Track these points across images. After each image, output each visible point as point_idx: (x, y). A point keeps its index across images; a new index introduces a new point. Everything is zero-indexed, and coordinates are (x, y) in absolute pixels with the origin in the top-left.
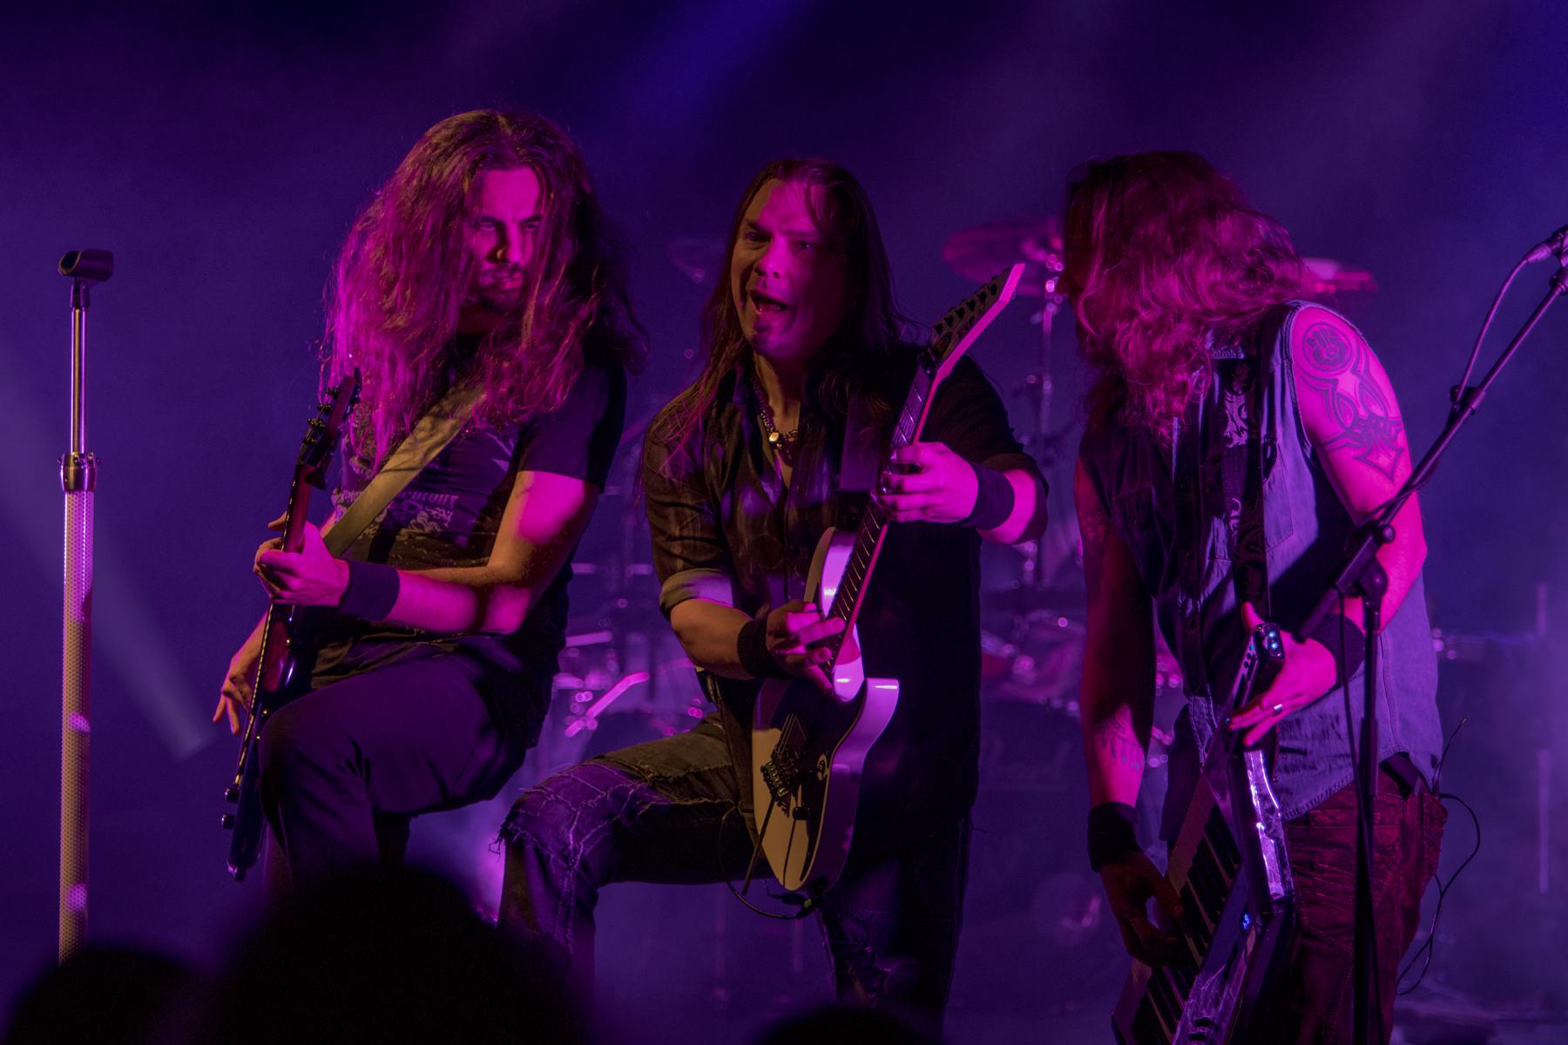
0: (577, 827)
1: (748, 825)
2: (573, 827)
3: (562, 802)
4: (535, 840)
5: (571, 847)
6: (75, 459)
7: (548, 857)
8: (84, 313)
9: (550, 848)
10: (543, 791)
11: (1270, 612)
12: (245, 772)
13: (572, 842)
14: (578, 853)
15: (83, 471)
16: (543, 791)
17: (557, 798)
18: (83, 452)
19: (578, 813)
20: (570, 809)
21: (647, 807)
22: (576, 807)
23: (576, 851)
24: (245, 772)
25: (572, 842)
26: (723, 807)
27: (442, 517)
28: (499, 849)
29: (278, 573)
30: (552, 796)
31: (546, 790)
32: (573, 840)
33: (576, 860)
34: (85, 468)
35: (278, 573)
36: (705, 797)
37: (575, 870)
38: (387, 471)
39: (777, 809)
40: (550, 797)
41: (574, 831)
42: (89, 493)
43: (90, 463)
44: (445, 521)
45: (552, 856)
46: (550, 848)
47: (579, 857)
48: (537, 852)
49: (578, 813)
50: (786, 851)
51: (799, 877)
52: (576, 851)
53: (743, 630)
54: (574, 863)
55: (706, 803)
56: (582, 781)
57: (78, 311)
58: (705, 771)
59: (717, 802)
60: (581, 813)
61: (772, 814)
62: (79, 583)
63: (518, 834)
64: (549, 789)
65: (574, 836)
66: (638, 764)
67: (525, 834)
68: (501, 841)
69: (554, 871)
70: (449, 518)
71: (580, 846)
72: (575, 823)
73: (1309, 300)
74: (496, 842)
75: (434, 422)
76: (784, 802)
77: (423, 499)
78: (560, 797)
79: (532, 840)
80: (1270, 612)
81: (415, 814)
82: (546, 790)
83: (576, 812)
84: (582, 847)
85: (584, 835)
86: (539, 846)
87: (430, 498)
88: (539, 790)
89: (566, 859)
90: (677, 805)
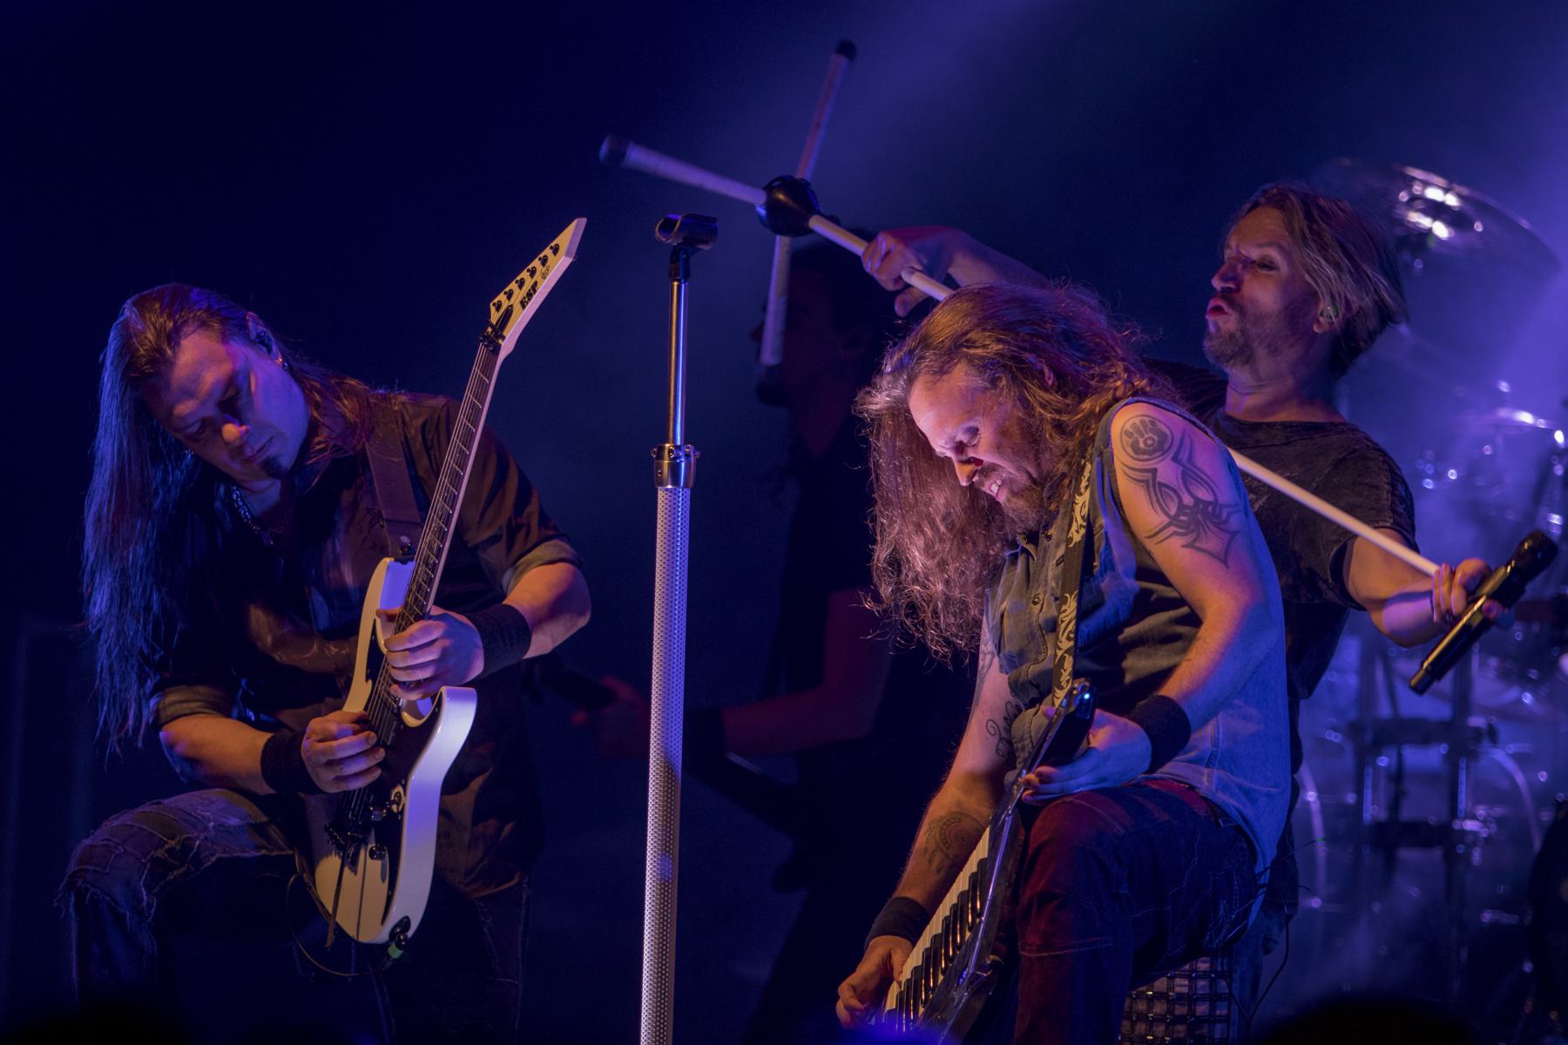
5: (144, 904)
6: (670, 451)
8: (683, 286)
10: (110, 843)
15: (679, 464)
16: (110, 843)
17: (125, 851)
18: (679, 443)
19: (148, 866)
21: (213, 859)
30: (120, 847)
33: (150, 914)
34: (681, 462)
38: (196, 422)
40: (117, 848)
42: (685, 490)
43: (687, 456)
49: (148, 866)
50: (364, 900)
51: (380, 922)
57: (676, 283)
62: (672, 573)
64: (116, 840)
66: (198, 811)
73: (758, 352)
90: (238, 857)
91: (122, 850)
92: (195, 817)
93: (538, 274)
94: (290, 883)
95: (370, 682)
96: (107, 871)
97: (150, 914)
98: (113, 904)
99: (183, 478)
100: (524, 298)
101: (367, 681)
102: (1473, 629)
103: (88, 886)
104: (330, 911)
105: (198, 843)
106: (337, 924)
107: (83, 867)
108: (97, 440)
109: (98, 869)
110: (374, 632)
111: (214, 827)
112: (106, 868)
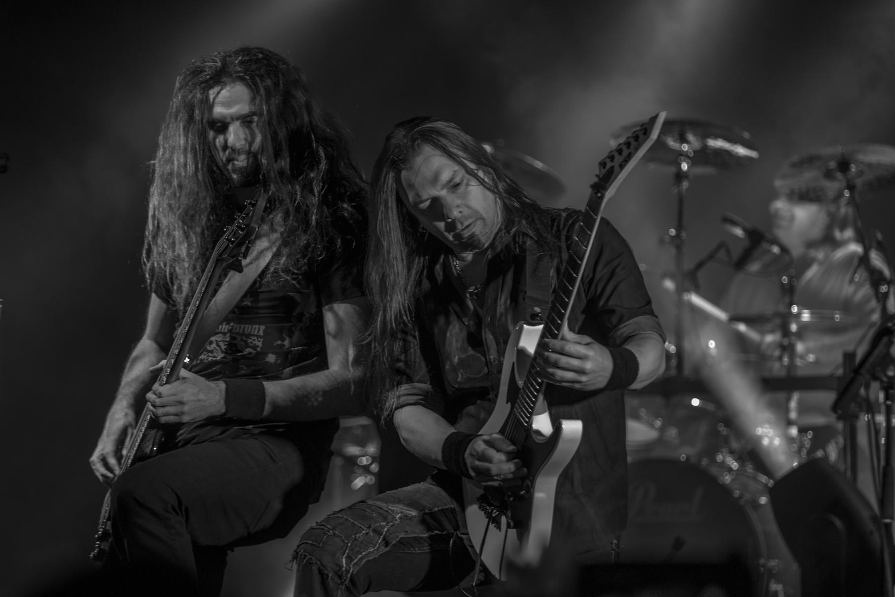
0: (348, 554)
1: (466, 542)
2: (346, 555)
3: (338, 536)
4: (319, 563)
5: (344, 569)
7: (328, 576)
9: (330, 570)
10: (325, 528)
11: (525, 199)
12: (111, 520)
13: (345, 565)
14: (348, 573)
16: (325, 528)
17: (334, 534)
19: (349, 544)
20: (344, 541)
22: (347, 540)
23: (347, 571)
24: (111, 520)
25: (345, 565)
26: (449, 536)
27: (255, 344)
28: (292, 567)
29: (510, 276)
30: (331, 531)
31: (326, 527)
32: (346, 563)
33: (347, 577)
35: (510, 276)
36: (436, 530)
37: (346, 585)
39: (492, 526)
40: (329, 532)
41: (346, 557)
44: (258, 346)
45: (330, 575)
46: (330, 570)
47: (349, 576)
48: (320, 572)
52: (347, 571)
53: (447, 439)
54: (345, 580)
55: (437, 534)
56: (352, 521)
58: (436, 512)
59: (444, 533)
60: (351, 544)
61: (480, 542)
63: (306, 559)
64: (329, 526)
65: (346, 561)
67: (311, 558)
68: (293, 561)
69: (331, 585)
70: (260, 344)
71: (350, 568)
72: (347, 551)
74: (290, 562)
75: (768, 241)
76: (496, 522)
77: (241, 332)
78: (336, 532)
79: (316, 564)
80: (525, 199)
81: (232, 545)
82: (326, 527)
83: (348, 544)
84: (352, 569)
85: (352, 560)
86: (321, 567)
87: (246, 330)
88: (322, 527)
89: (340, 577)
91: (332, 534)
92: (387, 511)
93: (632, 147)
94: (451, 546)
95: (509, 404)
96: (321, 545)
97: (347, 577)
98: (321, 567)
99: (313, 209)
100: (626, 158)
101: (507, 403)
102: (541, 401)
103: (307, 554)
104: (478, 551)
105: (386, 529)
106: (482, 562)
107: (305, 541)
108: (447, 343)
109: (315, 543)
110: (618, 265)
111: (400, 518)
112: (320, 544)
